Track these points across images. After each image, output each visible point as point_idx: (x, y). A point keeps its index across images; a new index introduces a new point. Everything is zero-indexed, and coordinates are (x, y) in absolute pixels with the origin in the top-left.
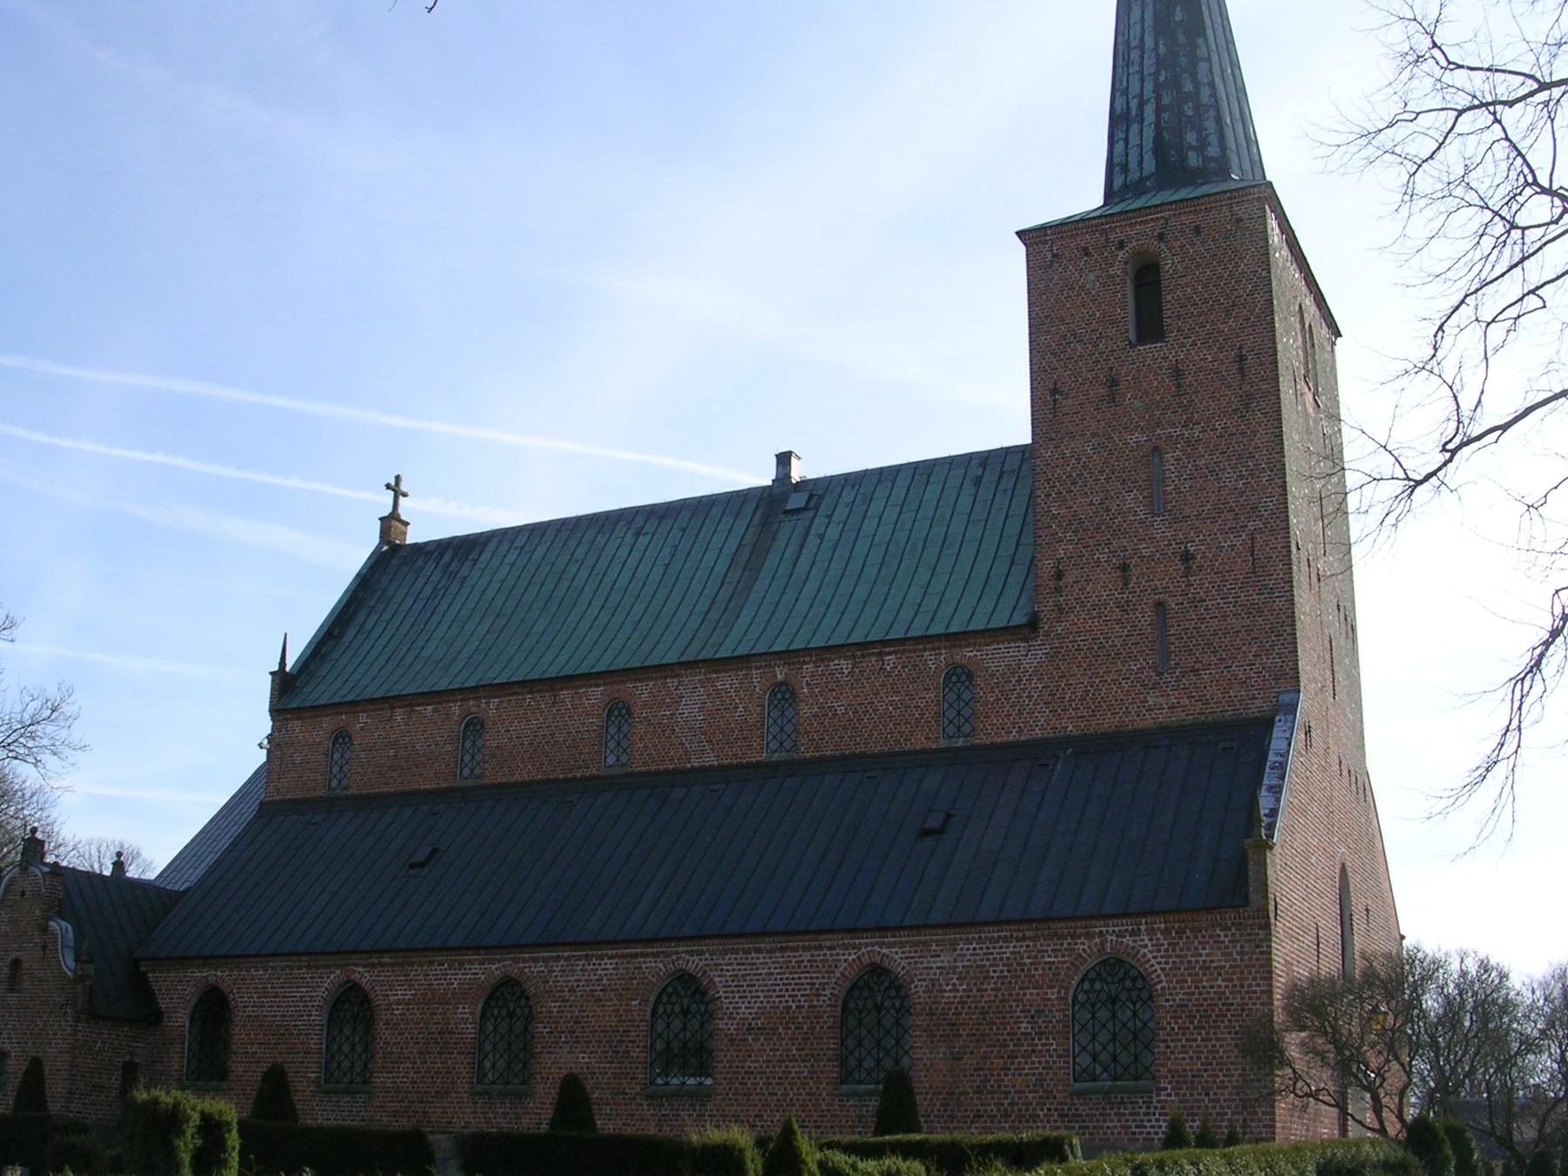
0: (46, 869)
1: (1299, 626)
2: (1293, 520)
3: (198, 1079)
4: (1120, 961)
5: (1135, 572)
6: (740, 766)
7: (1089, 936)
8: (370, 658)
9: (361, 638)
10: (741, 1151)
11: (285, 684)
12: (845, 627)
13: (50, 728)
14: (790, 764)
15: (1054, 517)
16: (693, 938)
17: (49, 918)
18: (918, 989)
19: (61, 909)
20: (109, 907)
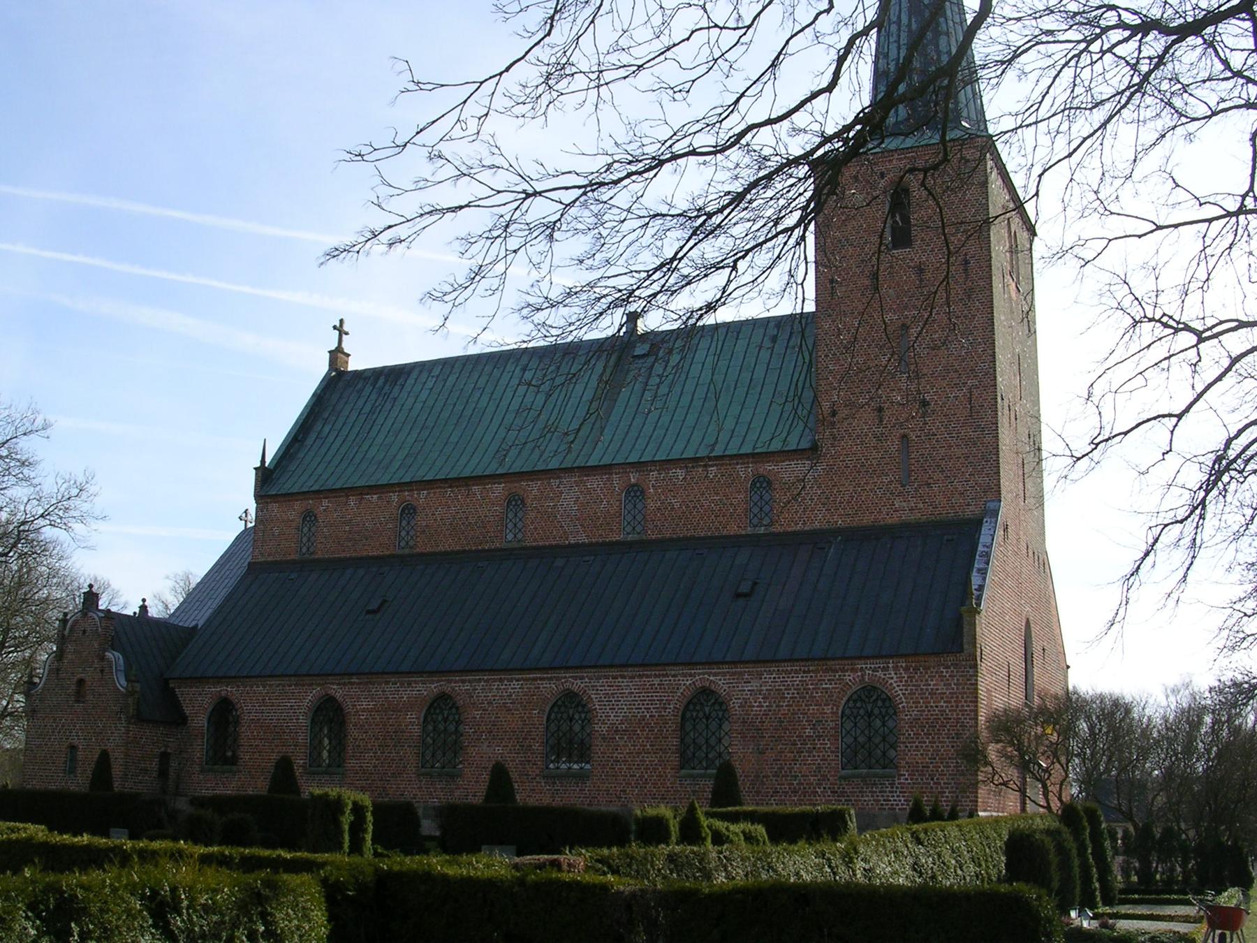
0: (101, 615)
1: (1001, 454)
2: (999, 379)
3: (215, 764)
4: (875, 688)
5: (887, 413)
6: (604, 544)
7: (853, 670)
8: (328, 458)
9: (319, 442)
10: (667, 820)
11: (266, 477)
12: (679, 446)
13: (77, 502)
14: (640, 543)
15: (831, 372)
16: (577, 668)
17: (105, 650)
18: (735, 704)
19: (114, 643)
20: (95, 628)
